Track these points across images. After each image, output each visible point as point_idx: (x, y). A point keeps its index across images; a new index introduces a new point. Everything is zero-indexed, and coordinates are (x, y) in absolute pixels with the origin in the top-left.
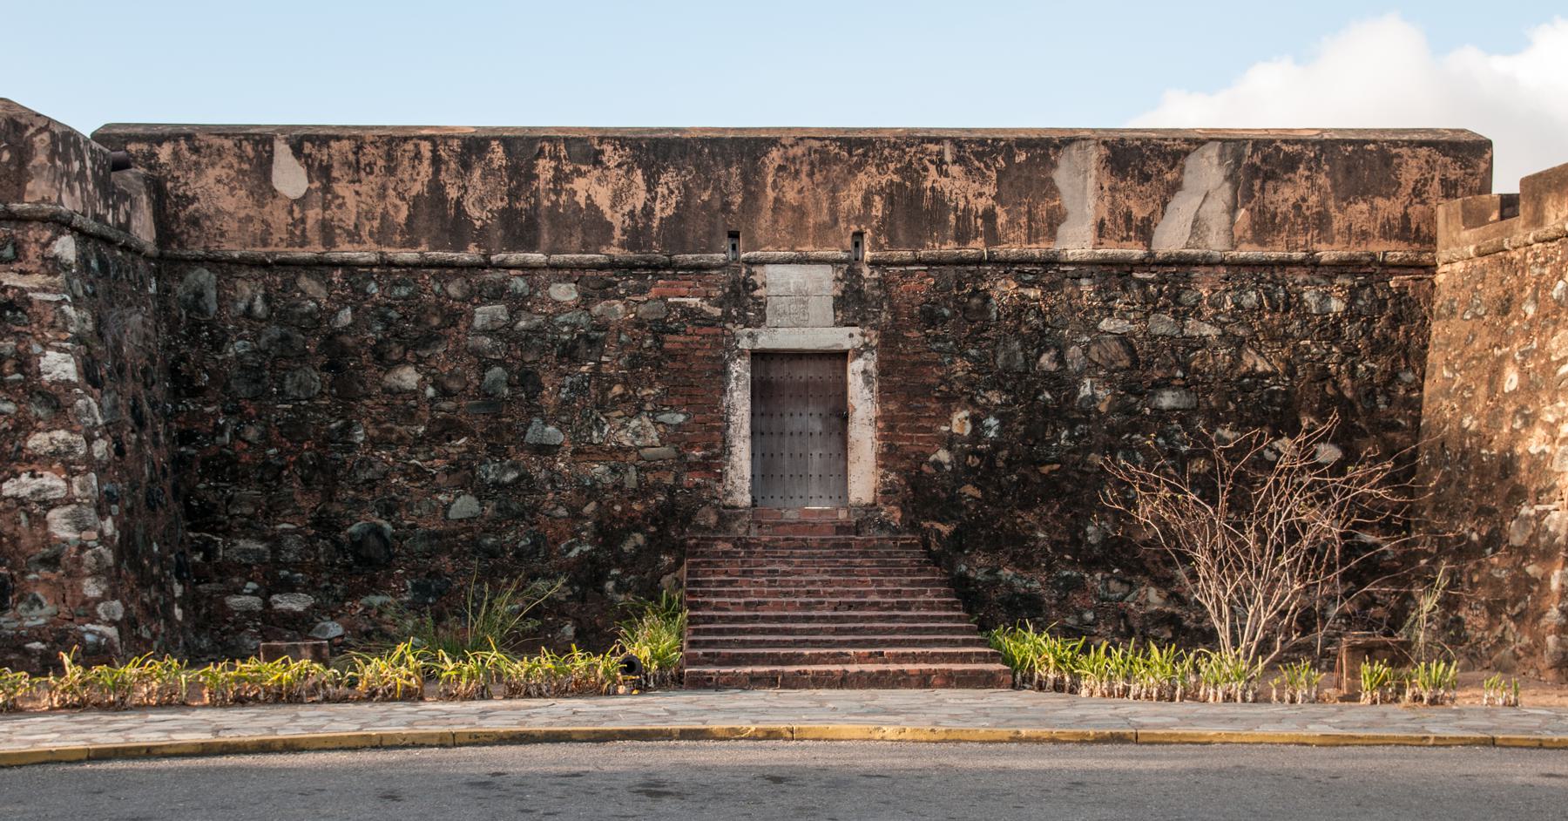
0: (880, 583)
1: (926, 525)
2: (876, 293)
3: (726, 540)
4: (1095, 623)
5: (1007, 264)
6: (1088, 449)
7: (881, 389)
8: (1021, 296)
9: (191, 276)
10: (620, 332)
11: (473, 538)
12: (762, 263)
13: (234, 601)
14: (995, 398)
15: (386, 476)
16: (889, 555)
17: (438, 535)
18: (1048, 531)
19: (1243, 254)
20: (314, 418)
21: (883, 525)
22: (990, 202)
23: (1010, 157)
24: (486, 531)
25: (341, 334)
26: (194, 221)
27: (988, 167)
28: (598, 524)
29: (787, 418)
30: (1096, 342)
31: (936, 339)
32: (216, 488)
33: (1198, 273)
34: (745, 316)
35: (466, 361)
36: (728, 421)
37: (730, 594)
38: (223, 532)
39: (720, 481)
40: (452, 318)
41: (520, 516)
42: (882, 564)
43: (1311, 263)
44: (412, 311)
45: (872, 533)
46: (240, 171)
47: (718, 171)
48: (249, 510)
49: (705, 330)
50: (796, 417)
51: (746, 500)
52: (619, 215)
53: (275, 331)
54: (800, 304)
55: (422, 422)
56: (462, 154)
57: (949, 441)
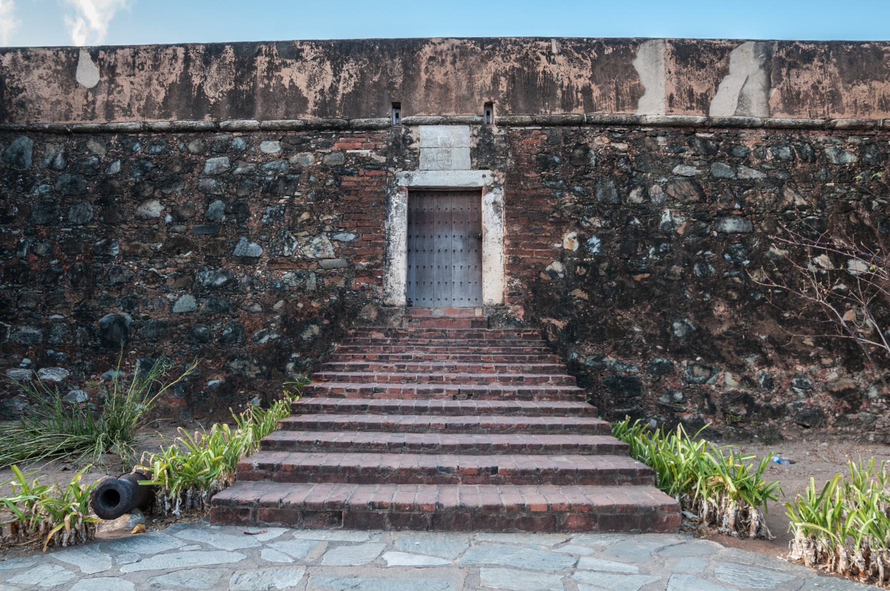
0: (503, 370)
1: (545, 320)
2: (503, 145)
3: (379, 331)
4: (683, 402)
5: (602, 125)
6: (671, 262)
7: (507, 215)
8: (612, 148)
9: (17, 141)
10: (309, 174)
11: (189, 328)
12: (417, 124)
13: (12, 372)
14: (596, 222)
15: (131, 279)
16: (514, 344)
17: (163, 325)
18: (642, 326)
19: (777, 120)
20: (86, 238)
21: (509, 320)
22: (587, 81)
23: (600, 50)
24: (200, 322)
25: (111, 178)
26: (22, 105)
27: (584, 57)
28: (284, 317)
29: (436, 239)
30: (672, 182)
31: (550, 179)
32: (12, 288)
33: (745, 133)
34: (404, 163)
35: (196, 196)
36: (389, 240)
37: (355, 379)
38: (11, 320)
39: (380, 284)
40: (189, 166)
41: (226, 310)
42: (506, 351)
43: (829, 128)
44: (163, 162)
45: (500, 326)
46: (56, 71)
47: (386, 68)
48: (32, 304)
49: (373, 173)
50: (443, 238)
51: (401, 300)
52: (312, 93)
53: (67, 178)
54: (445, 154)
55: (161, 240)
56: (205, 55)
57: (562, 255)
